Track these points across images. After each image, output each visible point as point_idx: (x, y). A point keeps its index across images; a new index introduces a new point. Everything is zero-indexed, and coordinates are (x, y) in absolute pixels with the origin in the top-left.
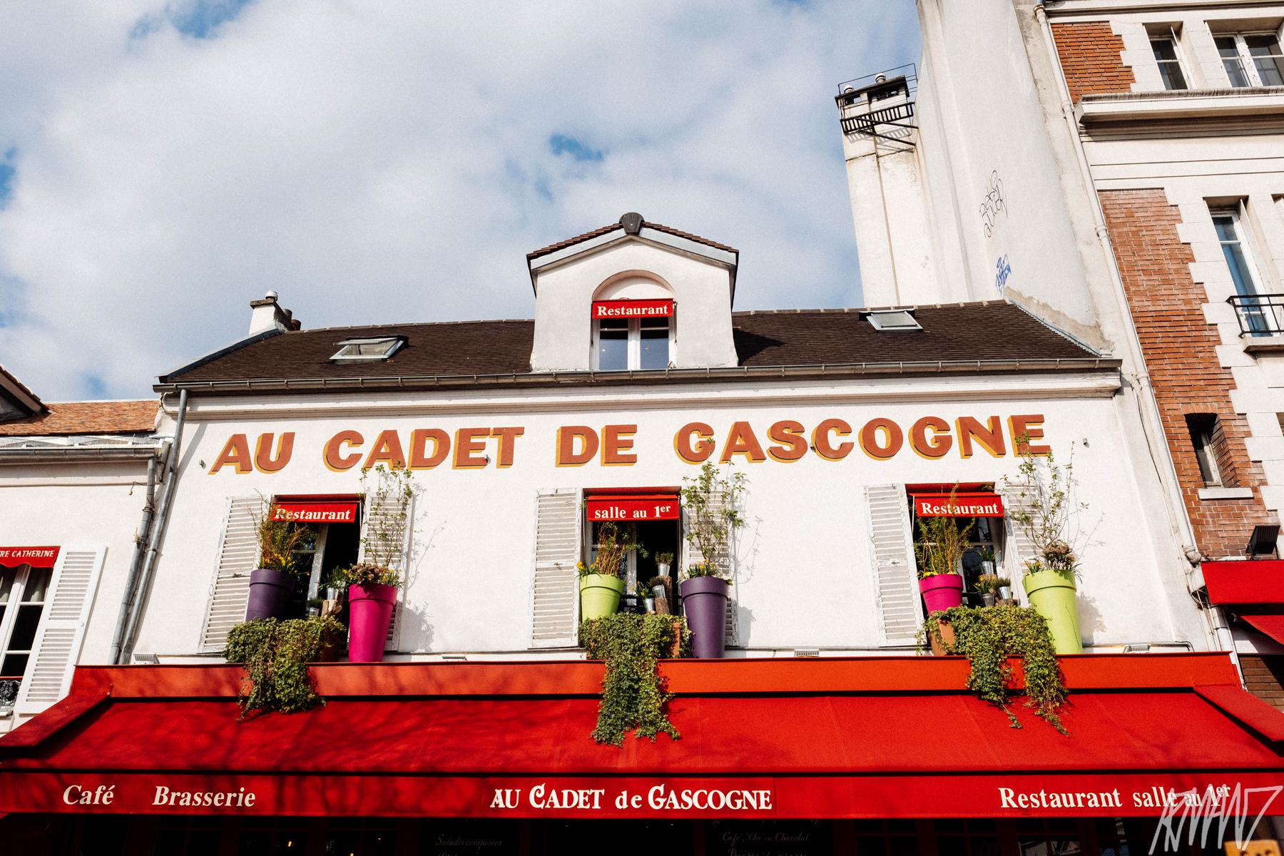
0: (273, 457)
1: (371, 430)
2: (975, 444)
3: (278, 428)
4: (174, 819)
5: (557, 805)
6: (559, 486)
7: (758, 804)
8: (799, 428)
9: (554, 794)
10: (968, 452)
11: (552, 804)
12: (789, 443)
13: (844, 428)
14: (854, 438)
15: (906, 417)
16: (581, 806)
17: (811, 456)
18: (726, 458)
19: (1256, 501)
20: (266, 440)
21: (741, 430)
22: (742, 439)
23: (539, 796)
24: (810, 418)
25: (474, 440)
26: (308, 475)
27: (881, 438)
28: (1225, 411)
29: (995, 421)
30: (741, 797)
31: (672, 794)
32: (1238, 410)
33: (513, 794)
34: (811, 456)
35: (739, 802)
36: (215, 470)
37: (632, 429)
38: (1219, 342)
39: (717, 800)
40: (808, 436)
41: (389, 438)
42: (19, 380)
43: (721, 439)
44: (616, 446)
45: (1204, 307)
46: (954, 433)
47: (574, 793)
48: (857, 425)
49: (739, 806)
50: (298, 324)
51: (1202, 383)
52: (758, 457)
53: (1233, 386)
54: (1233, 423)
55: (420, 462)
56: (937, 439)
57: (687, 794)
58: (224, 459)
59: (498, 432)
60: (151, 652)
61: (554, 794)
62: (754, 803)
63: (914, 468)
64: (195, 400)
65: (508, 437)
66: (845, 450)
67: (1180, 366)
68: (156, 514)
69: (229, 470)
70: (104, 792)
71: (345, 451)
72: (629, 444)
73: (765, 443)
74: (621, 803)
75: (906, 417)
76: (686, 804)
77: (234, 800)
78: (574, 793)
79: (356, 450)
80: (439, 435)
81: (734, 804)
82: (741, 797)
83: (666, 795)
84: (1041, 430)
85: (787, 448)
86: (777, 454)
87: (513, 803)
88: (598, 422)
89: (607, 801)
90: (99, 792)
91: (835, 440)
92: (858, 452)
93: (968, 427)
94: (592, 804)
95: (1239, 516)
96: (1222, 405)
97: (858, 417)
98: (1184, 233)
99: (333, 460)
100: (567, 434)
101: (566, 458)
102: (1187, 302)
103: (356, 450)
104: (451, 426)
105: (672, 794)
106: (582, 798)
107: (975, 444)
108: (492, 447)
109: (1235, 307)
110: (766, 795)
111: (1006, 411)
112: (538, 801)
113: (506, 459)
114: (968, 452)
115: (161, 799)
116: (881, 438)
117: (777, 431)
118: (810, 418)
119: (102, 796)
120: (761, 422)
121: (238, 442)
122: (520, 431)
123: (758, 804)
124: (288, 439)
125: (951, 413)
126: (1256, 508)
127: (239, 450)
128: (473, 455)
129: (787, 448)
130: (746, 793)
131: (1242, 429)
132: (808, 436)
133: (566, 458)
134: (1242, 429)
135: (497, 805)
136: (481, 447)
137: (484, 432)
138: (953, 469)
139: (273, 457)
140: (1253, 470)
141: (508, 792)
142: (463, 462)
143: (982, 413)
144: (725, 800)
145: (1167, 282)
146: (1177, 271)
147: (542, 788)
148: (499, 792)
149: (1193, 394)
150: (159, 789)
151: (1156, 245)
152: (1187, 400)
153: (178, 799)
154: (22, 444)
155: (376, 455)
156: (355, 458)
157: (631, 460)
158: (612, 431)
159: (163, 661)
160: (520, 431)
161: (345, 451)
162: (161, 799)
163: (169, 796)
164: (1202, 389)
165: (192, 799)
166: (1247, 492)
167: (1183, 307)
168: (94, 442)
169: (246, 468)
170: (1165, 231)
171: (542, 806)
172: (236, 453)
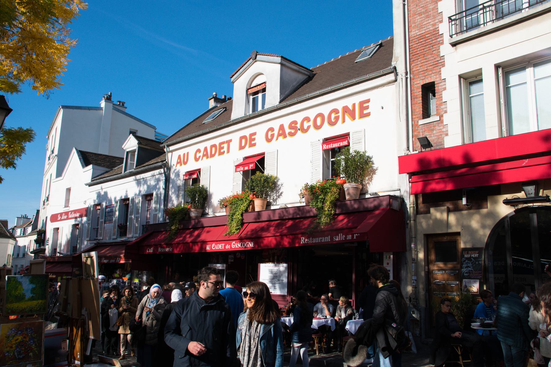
14: (311, 123)
17: (299, 132)
22: (282, 133)
25: (365, 105)
28: (438, 79)
37: (368, 101)
60: (375, 191)
65: (364, 105)
67: (425, 61)
69: (281, 138)
72: (367, 107)
85: (293, 131)
92: (312, 128)
93: (346, 109)
95: (433, 130)
114: (344, 121)
119: (151, 251)
122: (231, 141)
124: (188, 153)
132: (298, 126)
142: (221, 154)
143: (349, 102)
154: (142, 169)
155: (204, 155)
159: (381, 194)
160: (231, 141)
164: (431, 70)
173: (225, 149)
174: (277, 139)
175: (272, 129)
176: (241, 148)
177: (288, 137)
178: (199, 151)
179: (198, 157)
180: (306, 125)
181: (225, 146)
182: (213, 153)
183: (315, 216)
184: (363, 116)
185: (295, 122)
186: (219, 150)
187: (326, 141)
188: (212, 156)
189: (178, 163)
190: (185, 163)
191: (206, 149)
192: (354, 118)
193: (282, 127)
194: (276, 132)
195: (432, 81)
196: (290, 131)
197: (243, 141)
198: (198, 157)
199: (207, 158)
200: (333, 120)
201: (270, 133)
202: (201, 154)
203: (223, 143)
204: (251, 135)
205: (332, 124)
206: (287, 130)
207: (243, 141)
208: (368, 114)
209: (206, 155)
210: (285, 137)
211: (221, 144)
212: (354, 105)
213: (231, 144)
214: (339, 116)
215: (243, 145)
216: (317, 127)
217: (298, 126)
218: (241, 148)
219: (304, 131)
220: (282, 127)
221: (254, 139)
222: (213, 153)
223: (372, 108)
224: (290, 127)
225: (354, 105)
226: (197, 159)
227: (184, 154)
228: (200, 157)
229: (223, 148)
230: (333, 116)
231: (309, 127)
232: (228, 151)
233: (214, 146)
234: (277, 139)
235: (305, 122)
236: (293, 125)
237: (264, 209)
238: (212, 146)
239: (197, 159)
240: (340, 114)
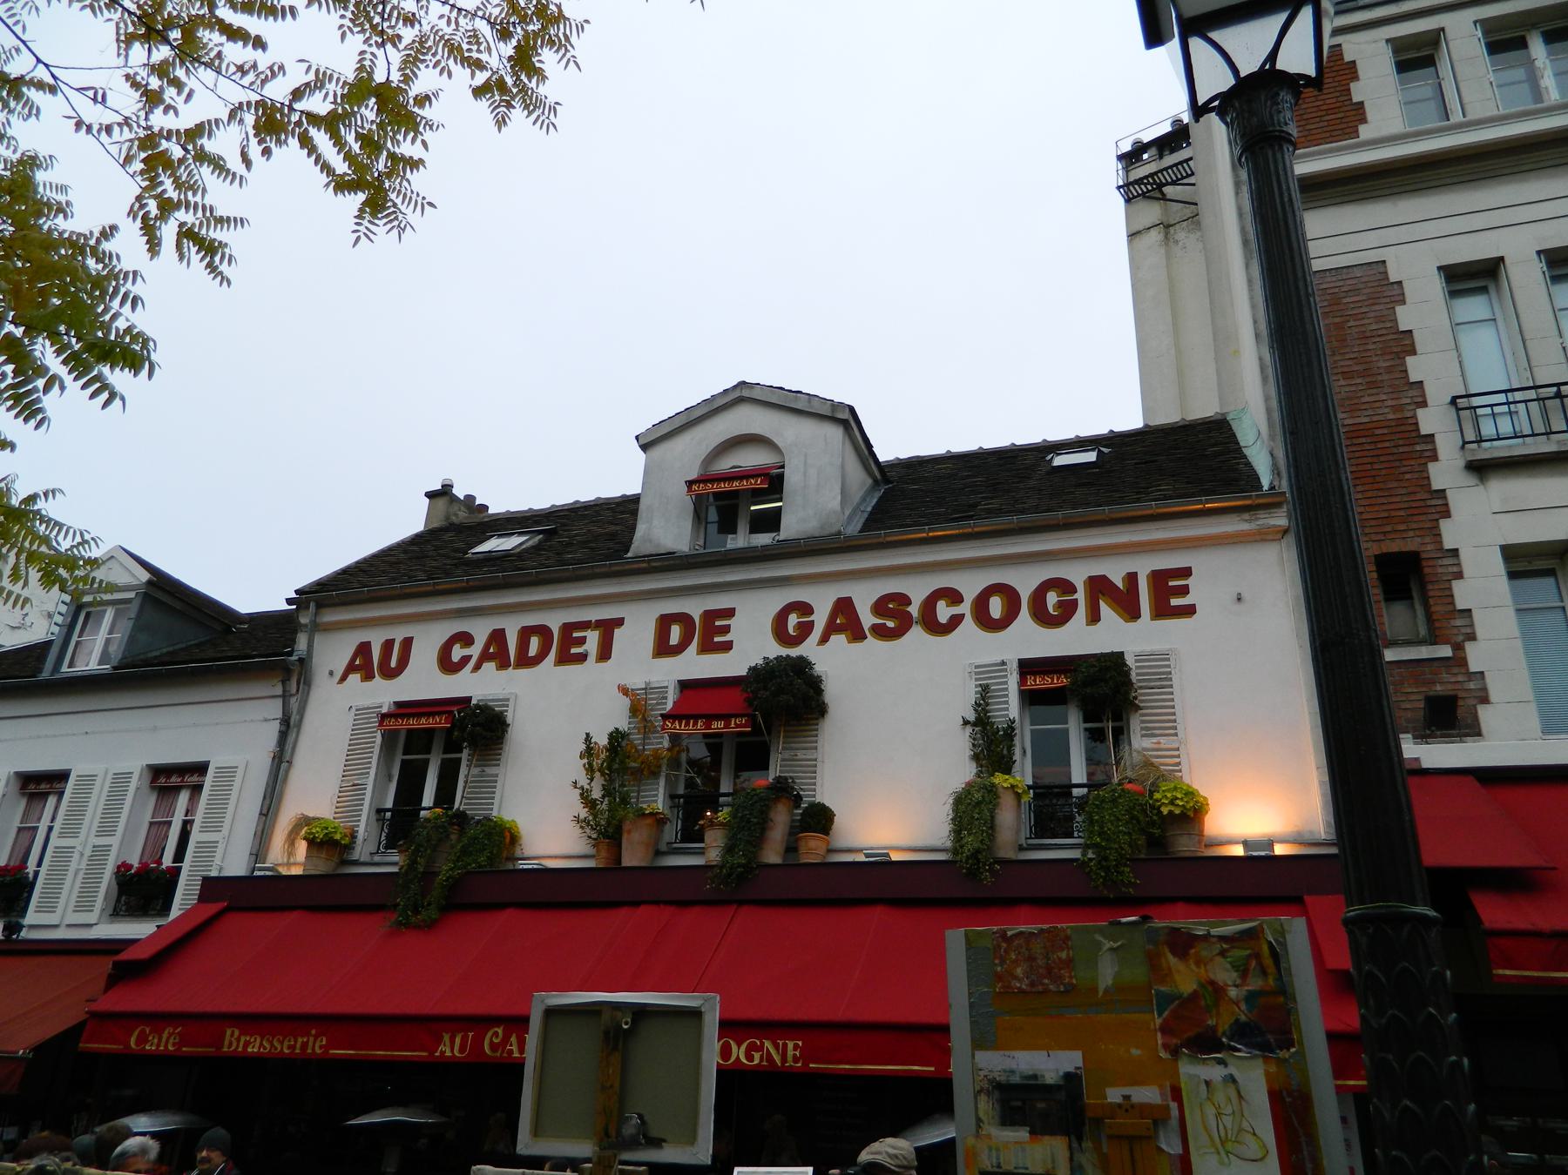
0: (393, 664)
1: (481, 631)
2: (1105, 609)
3: (398, 634)
4: (258, 1061)
5: (448, 1054)
6: (653, 679)
7: (784, 1059)
8: (904, 600)
9: (513, 1039)
10: (1094, 617)
11: (511, 1052)
12: (895, 617)
13: (954, 597)
14: (965, 608)
15: (1025, 582)
17: (916, 633)
18: (824, 639)
19: (1459, 661)
20: (388, 645)
21: (844, 607)
22: (845, 620)
24: (917, 590)
26: (422, 681)
27: (996, 607)
29: (1132, 578)
30: (760, 1048)
32: (1448, 545)
34: (916, 633)
35: (757, 1056)
36: (343, 678)
38: (1435, 458)
40: (914, 610)
41: (498, 637)
43: (820, 619)
44: (712, 633)
45: (1420, 413)
46: (1080, 596)
48: (970, 595)
50: (485, 508)
51: (1402, 513)
52: (857, 635)
53: (1447, 514)
54: (1440, 562)
55: (525, 661)
56: (1060, 604)
58: (351, 668)
59: (600, 624)
61: (513, 1039)
63: (1028, 639)
64: (324, 611)
65: (608, 628)
66: (956, 621)
68: (288, 728)
70: (170, 1035)
71: (457, 653)
72: (726, 630)
73: (868, 619)
75: (1025, 582)
77: (305, 1045)
79: (466, 652)
80: (543, 631)
82: (760, 1048)
83: (506, 1040)
84: (1187, 586)
85: (890, 624)
86: (881, 632)
87: (462, 1050)
88: (695, 608)
90: (165, 1035)
91: (944, 612)
92: (968, 623)
93: (1099, 586)
96: (1427, 540)
97: (970, 585)
98: (1406, 318)
99: (448, 665)
100: (665, 622)
101: (663, 648)
102: (1398, 408)
103: (466, 652)
104: (554, 621)
107: (1105, 609)
108: (593, 639)
109: (1458, 410)
110: (796, 1047)
111: (1144, 567)
113: (605, 653)
114: (1094, 617)
115: (230, 1044)
116: (996, 607)
117: (880, 607)
118: (917, 590)
120: (864, 597)
121: (364, 649)
123: (784, 1059)
124: (407, 643)
126: (1455, 670)
129: (890, 624)
130: (767, 1044)
131: (1451, 569)
132: (914, 610)
133: (663, 648)
134: (1451, 569)
135: (443, 1053)
136: (582, 641)
137: (585, 625)
138: (1077, 639)
139: (393, 664)
140: (1458, 622)
142: (565, 658)
143: (1115, 572)
145: (1373, 385)
146: (1389, 370)
147: (500, 1031)
148: (446, 1038)
149: (1389, 528)
150: (229, 1032)
151: (1365, 337)
152: (1380, 537)
153: (247, 1044)
156: (465, 660)
157: (728, 646)
158: (710, 616)
160: (619, 622)
161: (457, 653)
162: (230, 1044)
163: (238, 1040)
165: (261, 1045)
166: (1445, 651)
167: (1391, 416)
168: (1510, 446)
169: (368, 676)
170: (1380, 319)
172: (361, 664)
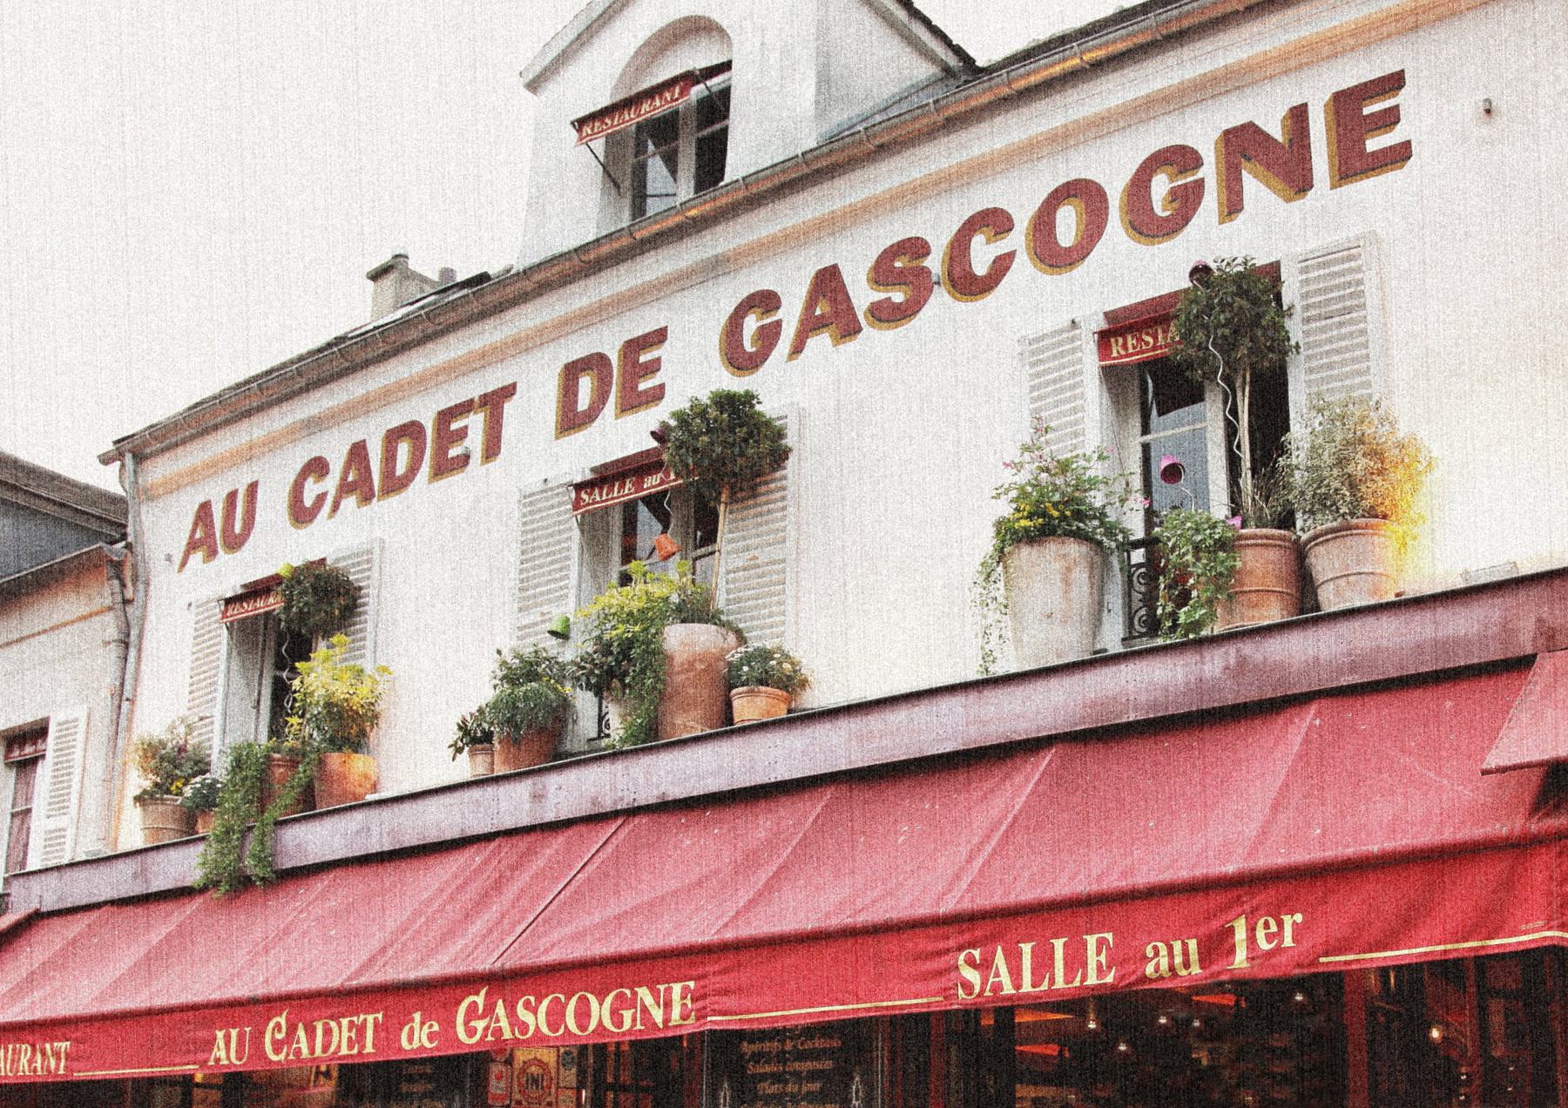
5: (305, 1052)
9: (301, 1033)
11: (298, 1052)
14: (1017, 240)
16: (344, 1051)
17: (941, 301)
22: (830, 307)
23: (279, 1036)
25: (644, 358)
31: (500, 1009)
33: (241, 1037)
34: (941, 301)
35: (627, 1015)
39: (583, 1014)
42: (1108, 11)
47: (333, 1024)
49: (627, 1024)
57: (527, 1005)
62: (658, 1015)
72: (1390, 119)
74: (410, 1040)
75: (1112, 168)
76: (524, 1028)
78: (333, 1024)
80: (1181, 158)
81: (619, 1023)
83: (490, 1009)
85: (898, 297)
89: (387, 1032)
92: (1023, 268)
93: (1243, 144)
94: (363, 1046)
105: (500, 1009)
106: (345, 1034)
112: (277, 1049)
122: (509, 391)
124: (253, 488)
125: (1202, 132)
127: (834, 301)
128: (1374, 144)
130: (644, 993)
132: (934, 263)
135: (218, 1060)
141: (234, 1033)
142: (445, 467)
144: (600, 1011)
155: (345, 488)
160: (509, 391)
171: (282, 1057)
173: (475, 441)
174: (797, 349)
175: (766, 301)
176: (571, 420)
177: (869, 332)
178: (317, 467)
179: (308, 502)
180: (982, 255)
181: (475, 423)
182: (401, 468)
183: (1355, 731)
184: (1353, 165)
185: (916, 248)
186: (439, 448)
187: (1118, 327)
188: (395, 484)
189: (192, 546)
190: (235, 543)
191: (358, 452)
192: (1296, 180)
193: (828, 282)
194: (790, 315)
195: (1273, 260)
196: (879, 296)
197: (586, 385)
198: (308, 502)
199: (367, 498)
200: (1160, 209)
201: (751, 324)
202: (331, 484)
203: (465, 408)
204: (635, 346)
205: (1147, 227)
206: (862, 295)
207: (586, 385)
208: (1400, 154)
209: (358, 485)
210: (850, 330)
211: (446, 416)
212: (1299, 115)
213: (509, 408)
214: (1200, 184)
215: (583, 403)
216: (1053, 257)
217: (934, 263)
218: (571, 420)
219: (968, 285)
220: (828, 282)
221: (654, 367)
222: (401, 468)
223: (1418, 113)
224: (882, 273)
225: (1299, 115)
226: (301, 514)
227: (232, 496)
228: (321, 498)
229: (462, 434)
230: (1161, 186)
231: (1002, 265)
232: (492, 449)
233: (411, 430)
234: (797, 349)
235: (978, 241)
236: (902, 267)
237: (1112, 638)
238: (393, 437)
239: (301, 514)
240: (1209, 172)
